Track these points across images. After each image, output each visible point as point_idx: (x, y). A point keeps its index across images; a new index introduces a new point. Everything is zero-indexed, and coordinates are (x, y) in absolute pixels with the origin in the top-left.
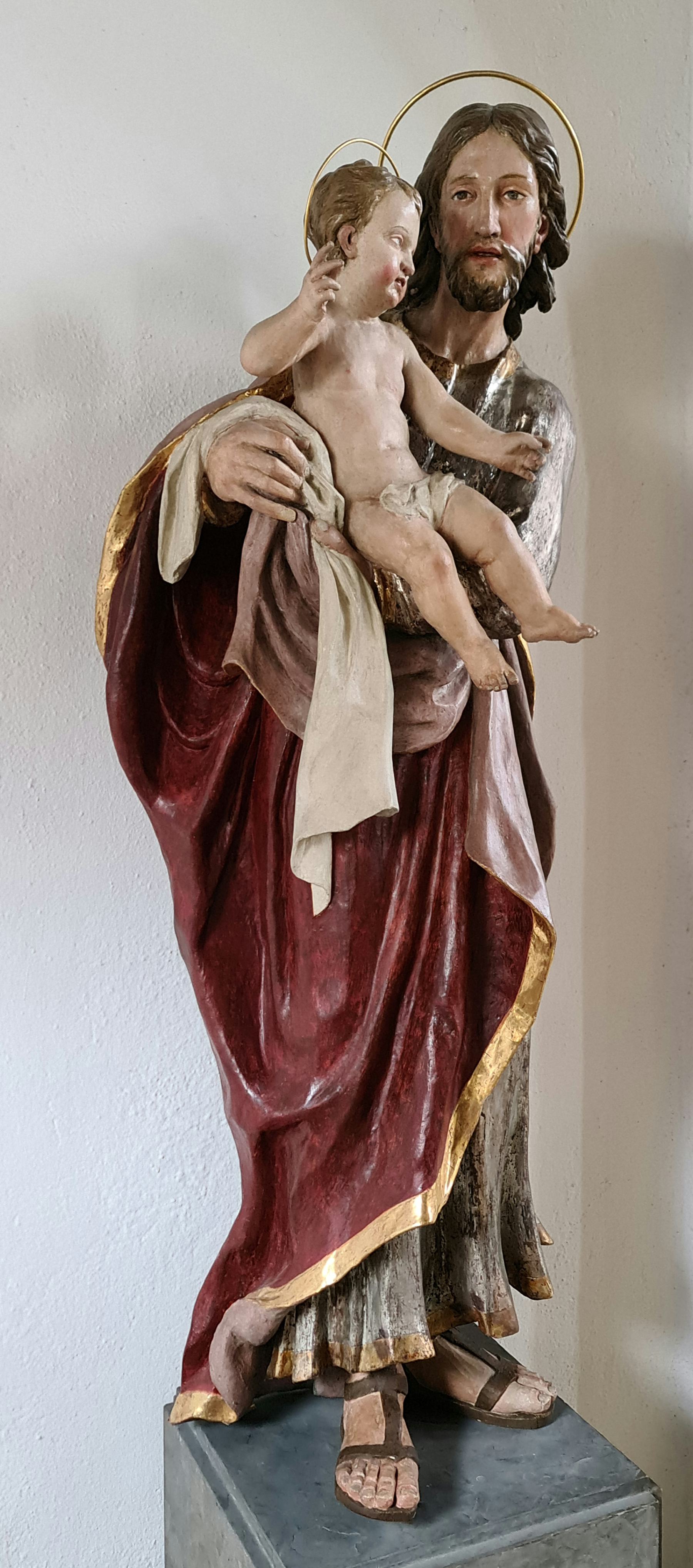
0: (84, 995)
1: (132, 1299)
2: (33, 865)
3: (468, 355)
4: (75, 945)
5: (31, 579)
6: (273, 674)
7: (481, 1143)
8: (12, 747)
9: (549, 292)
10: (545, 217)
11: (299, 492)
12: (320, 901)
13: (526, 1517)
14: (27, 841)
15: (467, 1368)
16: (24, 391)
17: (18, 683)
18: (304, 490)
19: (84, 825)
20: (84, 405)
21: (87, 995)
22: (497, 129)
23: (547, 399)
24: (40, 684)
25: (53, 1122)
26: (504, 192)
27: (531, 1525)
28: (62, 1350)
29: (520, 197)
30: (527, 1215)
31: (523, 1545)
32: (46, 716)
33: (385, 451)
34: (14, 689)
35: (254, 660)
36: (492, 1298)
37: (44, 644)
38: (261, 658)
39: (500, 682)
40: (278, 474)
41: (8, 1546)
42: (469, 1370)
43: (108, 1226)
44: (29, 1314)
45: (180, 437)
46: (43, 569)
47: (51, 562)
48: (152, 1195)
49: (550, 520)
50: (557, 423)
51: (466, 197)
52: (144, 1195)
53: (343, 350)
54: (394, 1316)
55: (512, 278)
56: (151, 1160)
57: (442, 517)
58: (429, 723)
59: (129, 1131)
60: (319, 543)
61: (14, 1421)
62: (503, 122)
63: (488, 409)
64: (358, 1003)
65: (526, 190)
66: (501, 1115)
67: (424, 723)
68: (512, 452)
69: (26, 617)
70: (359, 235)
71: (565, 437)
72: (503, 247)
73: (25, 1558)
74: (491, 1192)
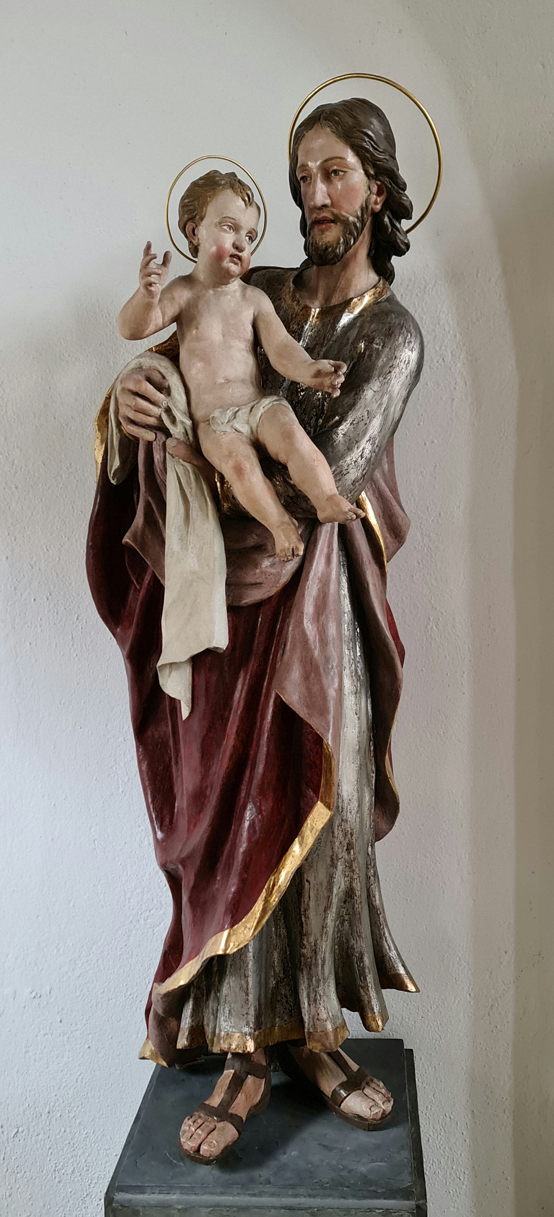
0: (113, 760)
1: (148, 970)
2: (78, 671)
4: (107, 726)
5: (76, 482)
7: (306, 902)
8: (65, 593)
10: (379, 183)
11: (160, 419)
12: (185, 712)
13: (301, 1191)
14: (75, 655)
15: (328, 1071)
18: (162, 416)
19: (112, 646)
20: (108, 362)
25: (94, 842)
26: (330, 172)
27: (305, 1197)
28: (101, 994)
29: (341, 173)
30: (360, 964)
31: (289, 1210)
33: (221, 384)
35: (143, 538)
36: (312, 1021)
38: (150, 537)
39: (288, 554)
40: (138, 409)
41: (69, 1113)
42: (329, 1073)
43: (131, 917)
44: (80, 965)
46: (84, 475)
47: (89, 470)
48: (161, 902)
49: (366, 424)
50: (392, 344)
52: (155, 901)
54: (226, 1017)
55: (346, 237)
56: (159, 877)
57: (257, 431)
58: (260, 583)
59: (144, 856)
60: (172, 455)
61: (72, 1032)
64: (207, 786)
65: (345, 167)
66: (325, 884)
67: (256, 584)
72: (333, 214)
73: (79, 1123)
74: (316, 941)
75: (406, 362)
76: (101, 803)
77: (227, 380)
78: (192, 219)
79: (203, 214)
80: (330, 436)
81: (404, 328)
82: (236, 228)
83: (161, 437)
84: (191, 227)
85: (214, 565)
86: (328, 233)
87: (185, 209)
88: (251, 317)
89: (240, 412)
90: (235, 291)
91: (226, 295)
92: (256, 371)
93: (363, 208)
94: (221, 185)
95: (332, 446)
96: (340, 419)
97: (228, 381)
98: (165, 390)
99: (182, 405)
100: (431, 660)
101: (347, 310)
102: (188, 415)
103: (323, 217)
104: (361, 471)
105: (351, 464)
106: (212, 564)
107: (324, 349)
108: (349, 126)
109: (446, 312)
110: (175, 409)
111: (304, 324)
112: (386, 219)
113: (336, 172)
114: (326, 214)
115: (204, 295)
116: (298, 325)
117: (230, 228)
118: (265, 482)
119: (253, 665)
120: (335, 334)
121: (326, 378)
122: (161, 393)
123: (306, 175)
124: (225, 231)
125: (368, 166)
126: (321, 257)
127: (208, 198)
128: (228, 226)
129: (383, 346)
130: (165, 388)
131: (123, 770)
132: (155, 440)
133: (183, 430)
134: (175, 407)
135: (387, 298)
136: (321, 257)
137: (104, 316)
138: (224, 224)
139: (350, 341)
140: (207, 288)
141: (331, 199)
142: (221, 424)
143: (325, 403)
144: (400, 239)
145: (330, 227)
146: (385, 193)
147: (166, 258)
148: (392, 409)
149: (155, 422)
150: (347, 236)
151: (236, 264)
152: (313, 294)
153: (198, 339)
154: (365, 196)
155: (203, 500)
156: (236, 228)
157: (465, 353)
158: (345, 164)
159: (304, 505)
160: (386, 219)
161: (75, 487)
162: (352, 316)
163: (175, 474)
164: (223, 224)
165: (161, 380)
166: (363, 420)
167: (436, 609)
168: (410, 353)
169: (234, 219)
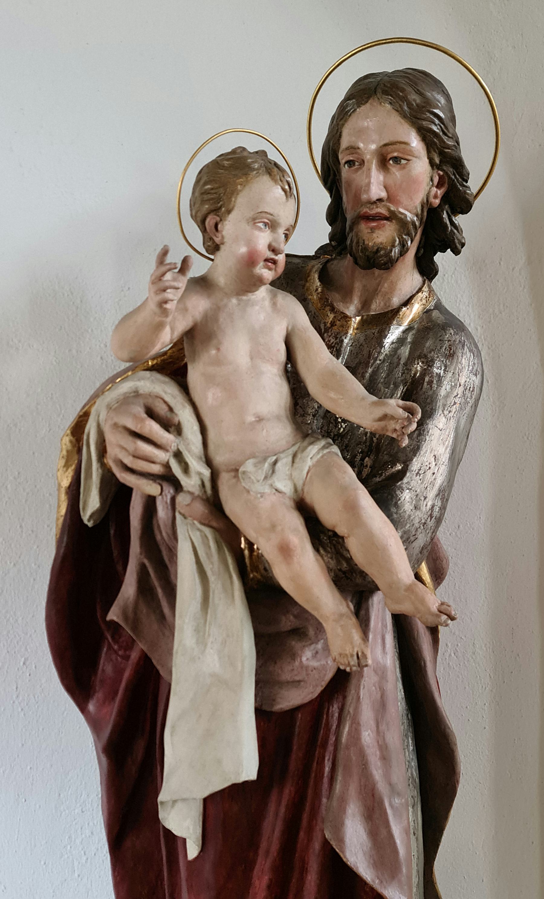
0: (67, 837)
3: (374, 303)
6: (155, 626)
8: (9, 632)
9: (81, 441)
10: (441, 173)
11: (167, 466)
14: (20, 710)
16: (20, 344)
17: (14, 579)
20: (70, 350)
21: (70, 837)
22: (379, 99)
23: (447, 344)
24: (32, 580)
26: (388, 158)
29: (403, 162)
32: (37, 606)
33: (251, 424)
34: (11, 585)
37: (35, 547)
38: (145, 611)
45: (93, 402)
46: (36, 486)
49: (434, 474)
50: (455, 369)
51: (354, 165)
53: (215, 328)
55: (402, 237)
57: (303, 490)
58: (299, 681)
62: (385, 93)
63: (384, 359)
65: (410, 155)
67: (294, 682)
68: (381, 419)
69: (21, 526)
70: (224, 223)
71: (462, 382)
72: (389, 210)
75: (471, 389)
76: (51, 891)
77: (259, 417)
78: (216, 211)
79: (231, 206)
80: (393, 493)
81: (466, 347)
82: (272, 225)
83: (169, 491)
84: (213, 222)
85: (243, 666)
86: (380, 232)
87: (206, 197)
88: (283, 333)
89: (279, 465)
90: (263, 299)
91: (253, 305)
92: (291, 400)
93: (424, 203)
94: (254, 169)
95: (396, 505)
96: (402, 468)
97: (260, 419)
98: (173, 428)
99: (197, 448)
100: (449, 692)
101: (395, 322)
102: (204, 459)
103: (377, 213)
104: (430, 534)
105: (420, 527)
106: (240, 665)
107: (370, 370)
108: (417, 105)
109: (467, 303)
110: (189, 456)
111: (343, 338)
112: (445, 215)
113: (397, 160)
114: (382, 210)
115: (226, 306)
116: (336, 339)
117: (265, 226)
118: (317, 560)
119: (288, 791)
120: (382, 351)
121: (391, 421)
122: (168, 431)
123: (355, 159)
124: (260, 229)
125: (434, 153)
126: (368, 259)
127: (239, 186)
128: (264, 222)
129: (445, 370)
130: (175, 425)
131: (80, 849)
132: (161, 494)
133: (199, 482)
134: (189, 452)
135: (435, 305)
136: (368, 259)
137: (66, 295)
138: (260, 220)
139: (402, 362)
140: (228, 295)
141: (387, 192)
142: (255, 481)
143: (374, 439)
144: (458, 240)
145: (384, 225)
146: (446, 185)
147: (185, 262)
148: (458, 449)
149: (160, 471)
150: (404, 237)
151: (270, 269)
152: (347, 296)
153: (218, 362)
154: (427, 188)
155: (227, 576)
156: (272, 225)
157: (487, 347)
158: (411, 151)
159: (359, 580)
160: (445, 215)
161: (24, 501)
162: (402, 328)
163: (189, 540)
164: (257, 221)
165: (169, 414)
166: (430, 468)
167: (454, 634)
168: (474, 378)
169: (272, 215)
